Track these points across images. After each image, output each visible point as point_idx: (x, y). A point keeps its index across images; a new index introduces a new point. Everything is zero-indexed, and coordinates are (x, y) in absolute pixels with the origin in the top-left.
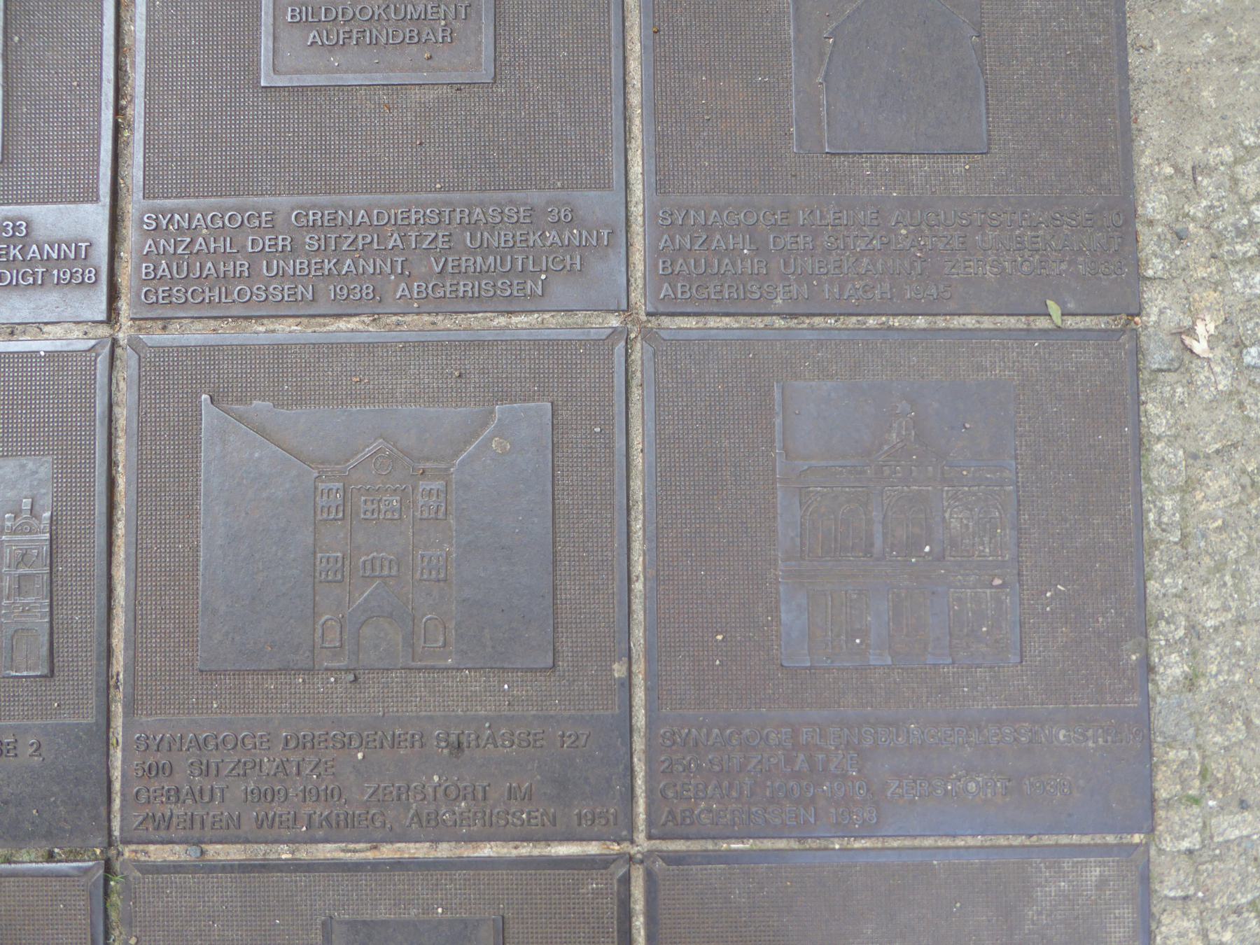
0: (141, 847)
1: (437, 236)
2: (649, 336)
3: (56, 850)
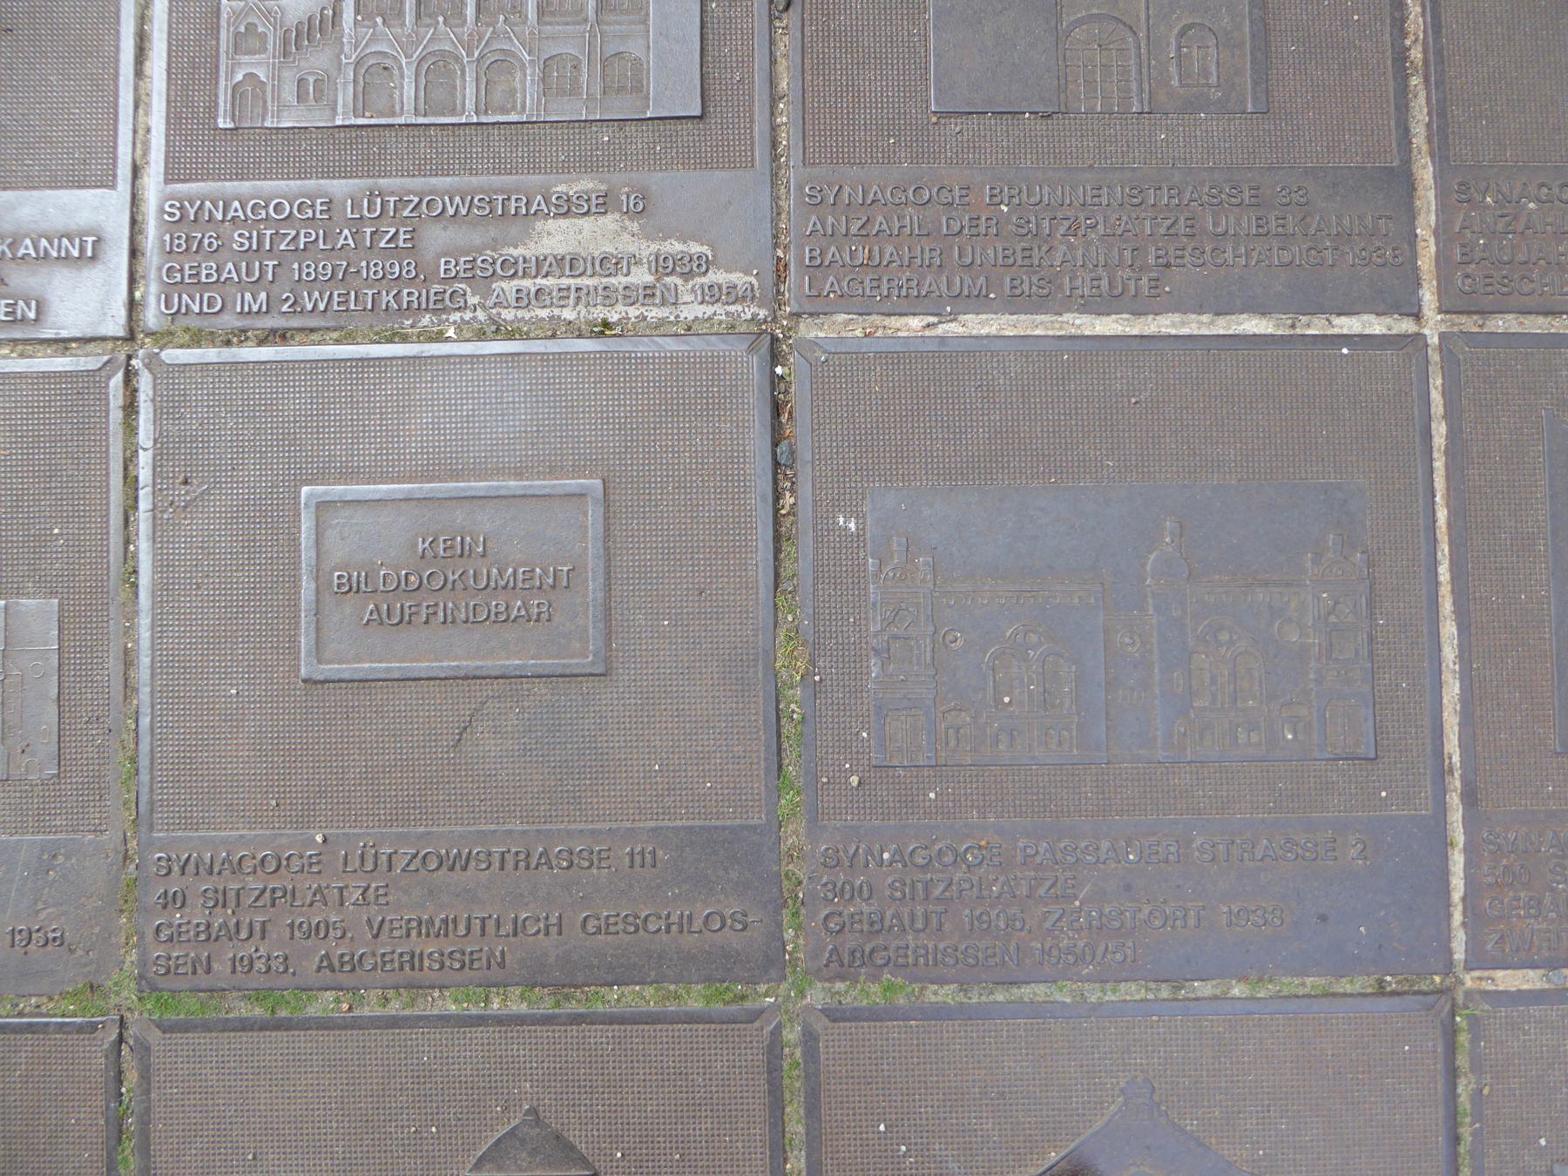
0: (1486, 973)
1: (397, 232)
2: (152, 362)
3: (1388, 978)
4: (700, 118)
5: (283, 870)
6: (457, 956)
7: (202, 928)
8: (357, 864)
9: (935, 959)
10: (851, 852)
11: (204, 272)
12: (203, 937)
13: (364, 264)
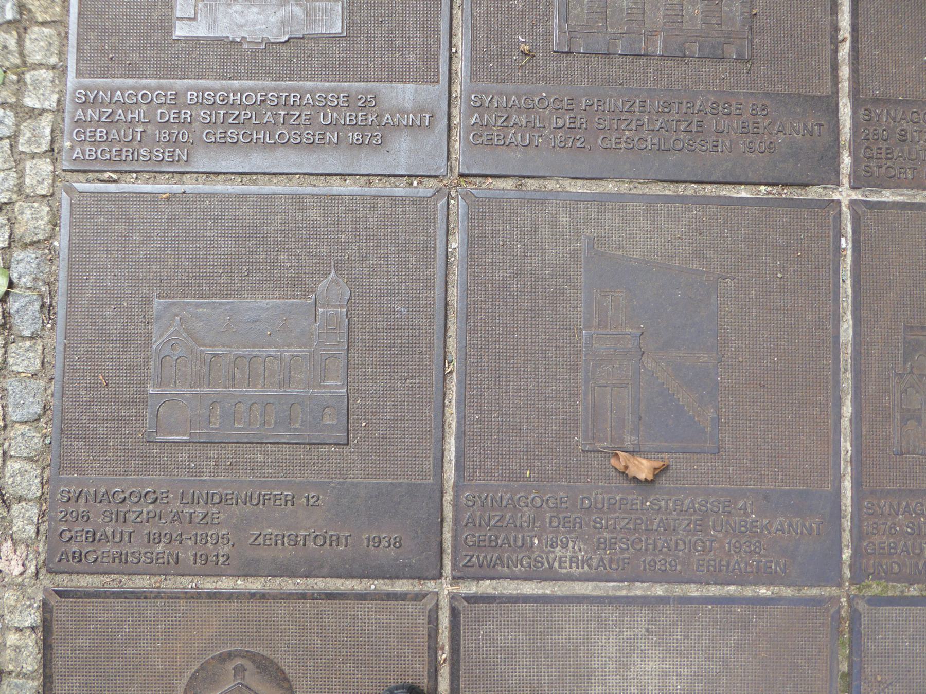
6: (149, 554)
10: (483, 497)
11: (99, 134)
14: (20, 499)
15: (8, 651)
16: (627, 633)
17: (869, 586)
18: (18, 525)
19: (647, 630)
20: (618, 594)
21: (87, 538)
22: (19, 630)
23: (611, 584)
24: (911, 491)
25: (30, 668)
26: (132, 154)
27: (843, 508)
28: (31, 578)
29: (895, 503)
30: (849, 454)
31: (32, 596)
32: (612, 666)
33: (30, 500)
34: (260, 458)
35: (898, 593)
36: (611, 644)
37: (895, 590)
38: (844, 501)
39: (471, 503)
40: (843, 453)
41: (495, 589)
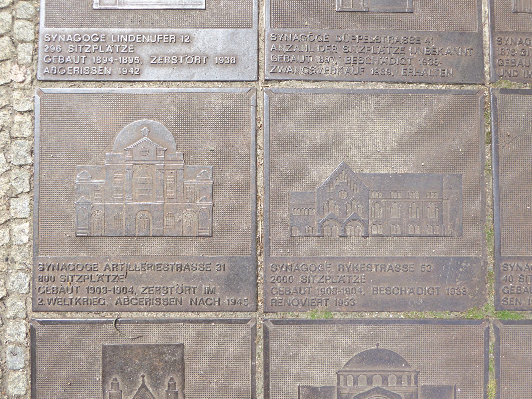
4: (205, 9)
5: (84, 269)
7: (55, 289)
8: (134, 267)
9: (91, 302)
12: (55, 292)
13: (120, 58)
14: (22, 42)
15: (16, 125)
16: (364, 110)
17: (500, 83)
18: (21, 55)
19: (375, 108)
20: (358, 88)
21: (53, 291)
22: (21, 113)
23: (354, 83)
24: (523, 32)
25: (28, 134)
26: (79, 70)
27: (484, 43)
28: (29, 84)
29: (514, 39)
30: (487, 13)
31: (29, 95)
32: (356, 128)
33: (28, 42)
34: (157, 18)
35: (517, 88)
36: (355, 116)
37: (516, 86)
38: (484, 39)
39: (274, 270)
40: (483, 13)
41: (288, 86)
